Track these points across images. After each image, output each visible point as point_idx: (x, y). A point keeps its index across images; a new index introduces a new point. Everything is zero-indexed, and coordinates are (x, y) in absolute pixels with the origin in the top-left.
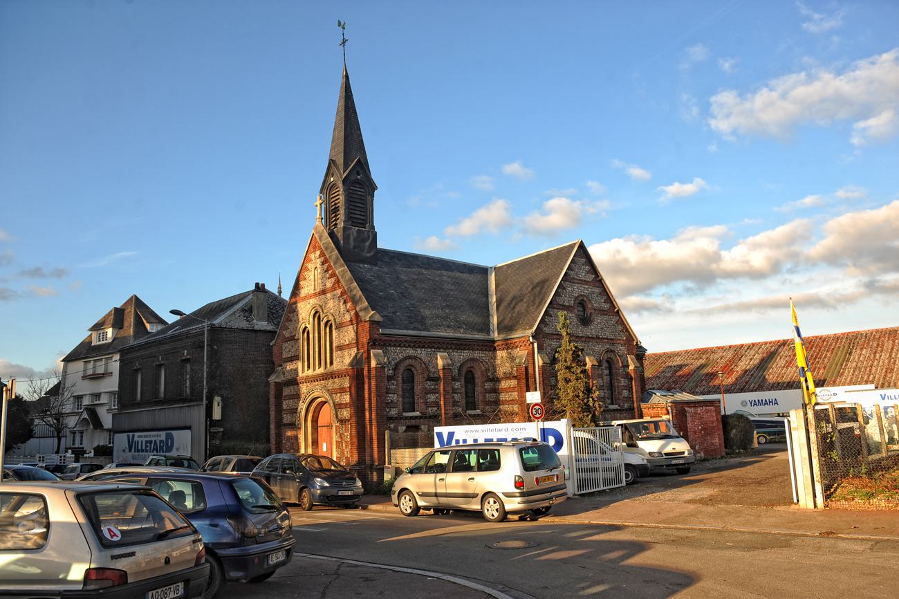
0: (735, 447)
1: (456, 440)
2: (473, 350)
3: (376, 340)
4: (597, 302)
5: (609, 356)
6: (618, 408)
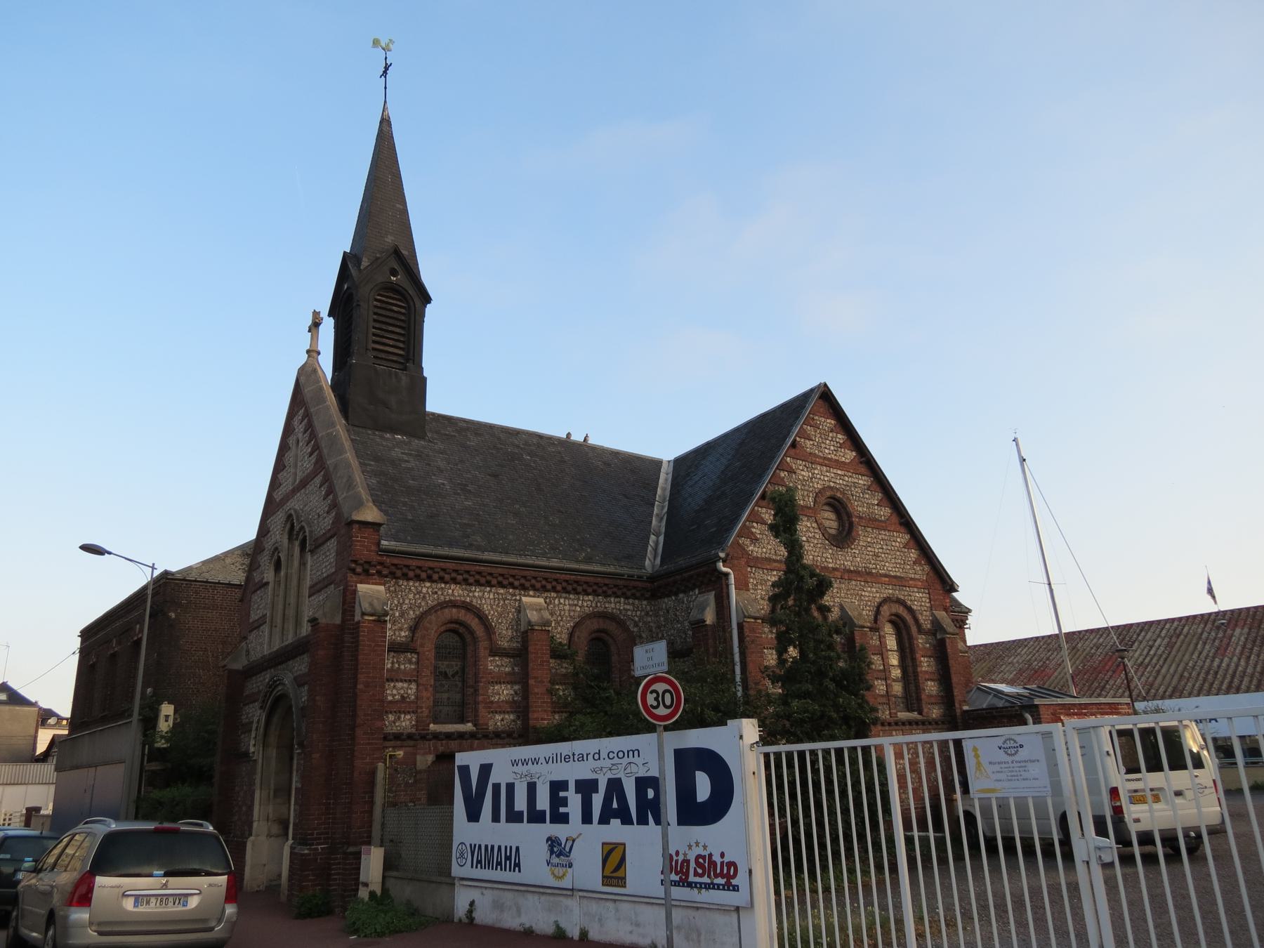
0: (161, 744)
1: (494, 785)
2: (606, 595)
3: (368, 563)
4: (865, 503)
5: (894, 611)
6: (919, 717)
